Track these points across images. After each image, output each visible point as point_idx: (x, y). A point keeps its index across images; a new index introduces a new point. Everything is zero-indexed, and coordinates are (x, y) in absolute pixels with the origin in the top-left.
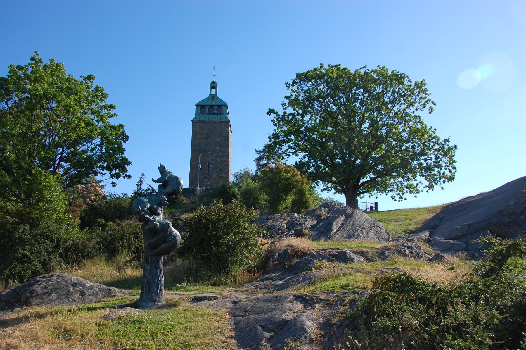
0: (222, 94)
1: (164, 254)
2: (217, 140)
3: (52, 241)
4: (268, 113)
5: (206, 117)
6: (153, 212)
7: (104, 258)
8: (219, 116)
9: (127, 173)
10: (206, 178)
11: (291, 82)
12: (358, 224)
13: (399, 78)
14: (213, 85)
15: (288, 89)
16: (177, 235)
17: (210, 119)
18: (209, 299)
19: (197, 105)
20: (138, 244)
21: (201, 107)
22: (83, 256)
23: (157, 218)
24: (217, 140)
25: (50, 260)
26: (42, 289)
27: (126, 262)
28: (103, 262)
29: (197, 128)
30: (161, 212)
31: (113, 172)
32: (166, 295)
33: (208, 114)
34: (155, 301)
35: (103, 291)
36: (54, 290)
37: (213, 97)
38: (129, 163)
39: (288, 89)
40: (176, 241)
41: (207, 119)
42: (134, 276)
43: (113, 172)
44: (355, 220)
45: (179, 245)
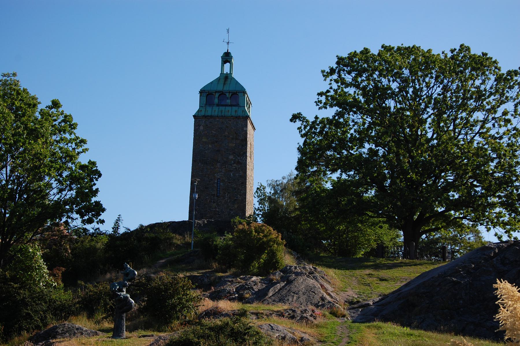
0: (241, 74)
2: (230, 145)
3: (46, 303)
4: (291, 120)
5: (215, 111)
8: (234, 108)
10: (214, 202)
11: (328, 70)
12: (294, 289)
13: (481, 64)
14: (227, 58)
15: (325, 80)
17: (220, 114)
19: (202, 92)
21: (207, 94)
22: (70, 314)
23: (122, 293)
24: (230, 145)
25: (46, 317)
27: (103, 318)
28: (85, 318)
29: (202, 128)
31: (86, 218)
32: (126, 334)
33: (218, 105)
34: (120, 336)
36: (67, 331)
37: (226, 78)
39: (325, 80)
41: (216, 114)
43: (86, 218)
44: (292, 286)
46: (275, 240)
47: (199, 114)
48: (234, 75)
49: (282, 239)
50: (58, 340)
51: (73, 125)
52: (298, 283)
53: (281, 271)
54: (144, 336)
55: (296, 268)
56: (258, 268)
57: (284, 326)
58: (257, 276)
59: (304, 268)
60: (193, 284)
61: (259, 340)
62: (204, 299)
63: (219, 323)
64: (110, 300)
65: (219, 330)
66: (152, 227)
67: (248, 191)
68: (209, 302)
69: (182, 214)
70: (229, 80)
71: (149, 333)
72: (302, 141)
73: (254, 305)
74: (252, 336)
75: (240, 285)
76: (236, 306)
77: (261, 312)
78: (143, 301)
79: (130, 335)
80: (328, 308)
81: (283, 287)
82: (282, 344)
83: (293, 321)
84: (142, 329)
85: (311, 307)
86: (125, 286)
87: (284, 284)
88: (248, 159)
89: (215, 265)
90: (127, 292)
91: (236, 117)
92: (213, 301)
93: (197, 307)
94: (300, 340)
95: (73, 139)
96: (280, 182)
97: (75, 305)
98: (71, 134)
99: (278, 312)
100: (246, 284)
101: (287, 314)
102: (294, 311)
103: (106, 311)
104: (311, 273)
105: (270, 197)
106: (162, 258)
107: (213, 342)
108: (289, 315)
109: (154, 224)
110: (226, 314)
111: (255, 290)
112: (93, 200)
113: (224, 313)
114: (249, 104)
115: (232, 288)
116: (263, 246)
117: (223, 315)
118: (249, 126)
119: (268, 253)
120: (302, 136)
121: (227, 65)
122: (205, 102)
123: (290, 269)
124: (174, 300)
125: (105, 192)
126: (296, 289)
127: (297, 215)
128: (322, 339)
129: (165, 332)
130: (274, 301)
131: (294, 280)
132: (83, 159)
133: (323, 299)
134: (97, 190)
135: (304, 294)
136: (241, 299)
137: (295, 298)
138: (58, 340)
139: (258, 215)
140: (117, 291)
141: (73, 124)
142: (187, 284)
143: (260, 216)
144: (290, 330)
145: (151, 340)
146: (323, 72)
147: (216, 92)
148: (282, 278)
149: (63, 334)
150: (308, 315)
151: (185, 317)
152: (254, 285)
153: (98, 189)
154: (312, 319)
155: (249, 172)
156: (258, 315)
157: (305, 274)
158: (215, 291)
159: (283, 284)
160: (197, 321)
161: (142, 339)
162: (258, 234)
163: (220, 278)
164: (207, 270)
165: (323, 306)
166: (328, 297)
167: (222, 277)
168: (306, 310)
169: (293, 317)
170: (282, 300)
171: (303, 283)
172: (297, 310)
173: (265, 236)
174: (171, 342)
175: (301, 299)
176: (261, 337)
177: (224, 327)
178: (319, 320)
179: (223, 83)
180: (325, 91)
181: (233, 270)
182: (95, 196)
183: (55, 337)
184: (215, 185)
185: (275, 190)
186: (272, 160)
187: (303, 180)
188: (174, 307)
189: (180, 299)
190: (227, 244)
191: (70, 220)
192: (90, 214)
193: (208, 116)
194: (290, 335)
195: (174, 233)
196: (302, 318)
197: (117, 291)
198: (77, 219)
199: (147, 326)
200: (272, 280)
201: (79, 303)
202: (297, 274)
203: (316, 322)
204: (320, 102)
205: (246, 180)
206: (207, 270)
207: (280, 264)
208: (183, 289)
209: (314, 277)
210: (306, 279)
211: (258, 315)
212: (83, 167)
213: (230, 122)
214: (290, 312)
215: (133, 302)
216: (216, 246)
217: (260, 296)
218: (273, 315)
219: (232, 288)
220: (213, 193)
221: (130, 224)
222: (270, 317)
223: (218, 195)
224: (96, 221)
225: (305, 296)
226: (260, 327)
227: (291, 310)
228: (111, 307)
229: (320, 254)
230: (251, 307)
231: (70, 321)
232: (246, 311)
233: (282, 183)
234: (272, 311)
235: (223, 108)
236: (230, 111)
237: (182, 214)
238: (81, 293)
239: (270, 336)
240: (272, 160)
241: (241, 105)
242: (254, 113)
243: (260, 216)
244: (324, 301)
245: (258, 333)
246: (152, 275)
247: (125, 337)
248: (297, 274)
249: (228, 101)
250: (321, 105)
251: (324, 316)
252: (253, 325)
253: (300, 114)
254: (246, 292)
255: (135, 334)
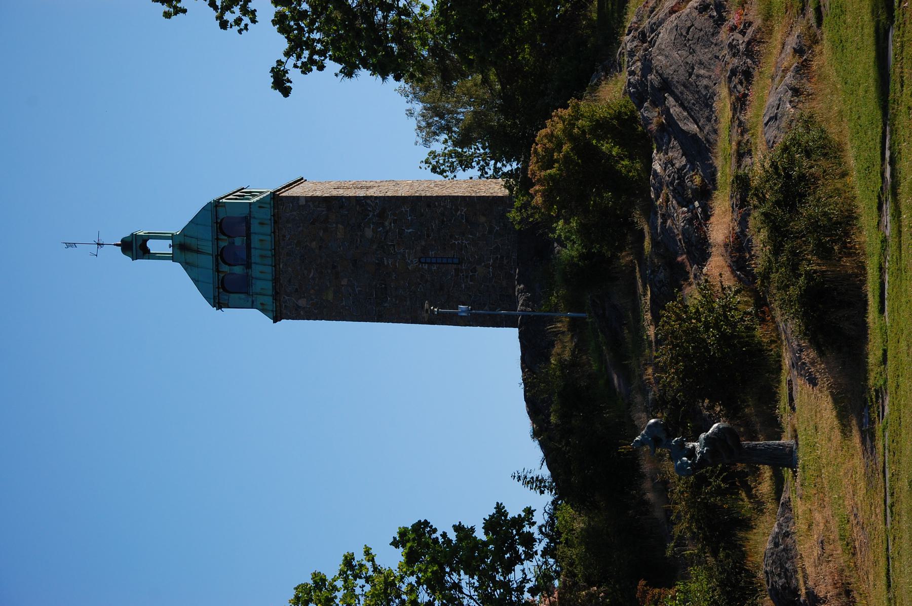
1: (739, 441)
4: (286, 92)
5: (262, 275)
6: (691, 453)
8: (255, 227)
12: (682, 75)
14: (135, 247)
16: (718, 427)
17: (269, 261)
19: (218, 304)
20: (717, 477)
21: (223, 292)
22: (742, 569)
23: (698, 449)
26: (780, 578)
27: (750, 496)
29: (302, 302)
30: (691, 445)
31: (521, 549)
32: (786, 440)
33: (248, 265)
36: (782, 567)
37: (184, 248)
40: (723, 428)
41: (269, 269)
42: (771, 479)
44: (676, 78)
46: (569, 124)
48: (177, 229)
49: (566, 107)
50: (801, 582)
52: (667, 67)
53: (640, 106)
54: (791, 399)
55: (632, 73)
56: (631, 158)
57: (768, 94)
58: (651, 160)
59: (632, 54)
61: (800, 145)
63: (764, 234)
64: (710, 483)
65: (779, 233)
66: (536, 406)
67: (445, 193)
68: (713, 264)
69: (505, 342)
70: (188, 241)
73: (719, 163)
74: (792, 161)
77: (734, 147)
79: (788, 431)
81: (677, 99)
83: (756, 73)
85: (724, 35)
86: (681, 445)
87: (671, 99)
88: (371, 193)
89: (626, 258)
90: (696, 439)
91: (275, 222)
92: (709, 255)
93: (723, 289)
96: (420, 118)
98: (335, 588)
99: (734, 109)
100: (672, 183)
101: (739, 87)
102: (734, 72)
103: (732, 490)
104: (643, 37)
106: (610, 381)
108: (741, 83)
109: (528, 406)
110: (740, 223)
111: (683, 163)
112: (480, 534)
113: (737, 229)
114: (242, 193)
115: (681, 214)
118: (296, 191)
121: (152, 245)
122: (243, 296)
123: (634, 86)
125: (458, 509)
126: (682, 70)
127: (497, 75)
129: (780, 356)
130: (709, 119)
131: (660, 75)
132: (392, 559)
134: (458, 528)
135: (692, 52)
136: (705, 193)
137: (702, 72)
138: (801, 582)
139: (496, 170)
140: (694, 461)
141: (315, 582)
142: (674, 312)
143: (499, 165)
144: (778, 78)
147: (218, 271)
148: (654, 104)
149: (788, 575)
150: (741, 41)
151: (746, 313)
152: (673, 165)
153: (454, 526)
154: (750, 32)
155: (403, 192)
157: (646, 50)
159: (671, 101)
161: (797, 402)
163: (655, 243)
164: (638, 275)
167: (653, 240)
168: (731, 46)
169: (748, 75)
170: (707, 101)
171: (667, 56)
172: (730, 67)
174: (805, 334)
175: (705, 58)
177: (774, 222)
179: (195, 255)
180: (214, 14)
183: (795, 592)
184: (435, 268)
186: (370, 137)
187: (421, 65)
188: (724, 339)
189: (707, 326)
190: (578, 231)
191: (528, 586)
193: (274, 288)
194: (789, 79)
195: (548, 360)
196: (749, 53)
197: (694, 461)
198: (523, 571)
199: (769, 397)
200: (661, 125)
201: (715, 554)
202: (647, 67)
203: (758, 22)
205: (420, 197)
206: (638, 275)
207: (623, 109)
208: (684, 321)
210: (659, 49)
212: (411, 558)
213: (288, 237)
214: (735, 80)
217: (698, 151)
218: (742, 118)
219: (681, 214)
220: (453, 272)
221: (532, 458)
223: (456, 261)
225: (698, 48)
226: (770, 145)
227: (730, 78)
229: (591, 19)
230: (725, 171)
232: (737, 177)
234: (732, 121)
236: (262, 237)
237: (505, 342)
239: (792, 121)
240: (370, 137)
242: (264, 182)
243: (499, 165)
245: (785, 149)
246: (650, 396)
247: (793, 441)
248: (647, 67)
249: (238, 241)
252: (767, 160)
254: (689, 184)
255: (786, 420)
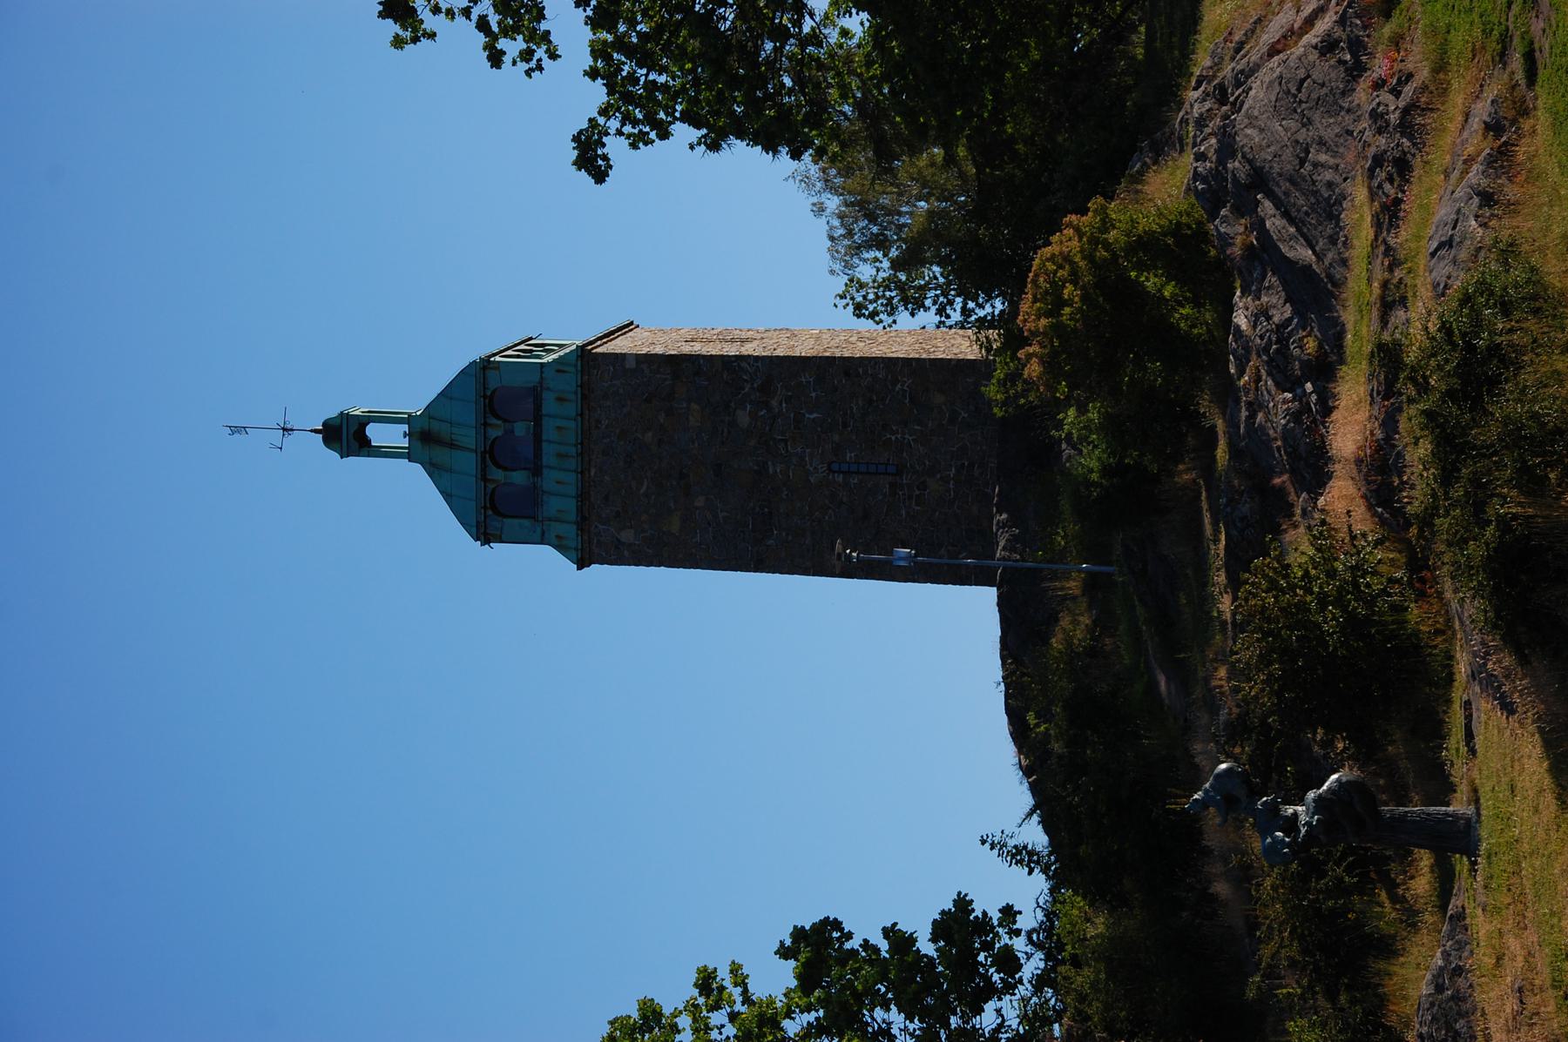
4: (600, 176)
5: (560, 484)
6: (1291, 824)
7: (1382, 965)
8: (549, 405)
9: (995, 916)
14: (347, 435)
15: (432, 36)
16: (1338, 780)
18: (1469, 718)
19: (485, 535)
21: (493, 515)
23: (1303, 818)
27: (1395, 899)
29: (627, 536)
30: (1290, 810)
32: (1459, 806)
33: (537, 470)
35: (1453, 930)
36: (1449, 1027)
37: (428, 439)
38: (963, 903)
40: (1348, 782)
41: (571, 478)
44: (1277, 169)
45: (1356, 773)
47: (572, 544)
48: (417, 407)
49: (1083, 211)
51: (644, 1017)
53: (1213, 215)
55: (1200, 157)
56: (1197, 304)
57: (1437, 201)
58: (1230, 309)
59: (1201, 123)
60: (1266, 554)
61: (1492, 294)
62: (1323, 511)
63: (1424, 449)
65: (1451, 449)
67: (876, 352)
68: (1335, 492)
69: (968, 617)
70: (435, 426)
71: (1457, 716)
72: (684, 133)
73: (1349, 317)
74: (1477, 322)
75: (1269, 374)
76: (1353, 394)
78: (1328, 744)
80: (1365, 27)
81: (1278, 204)
82: (1509, 204)
83: (1417, 162)
84: (1440, 748)
85: (1362, 95)
86: (1273, 809)
87: (1268, 204)
88: (749, 349)
89: (1185, 475)
90: (1300, 801)
91: (584, 397)
92: (1330, 476)
93: (1353, 538)
94: (1497, 137)
95: (695, 1020)
96: (836, 223)
97: (1342, 1010)
99: (1377, 225)
100: (1266, 349)
101: (1387, 186)
102: (1378, 161)
104: (1221, 95)
105: (896, 265)
106: (1153, 685)
107: (1499, 466)
108: (1391, 180)
110: (1383, 425)
111: (1288, 315)
112: (926, 947)
113: (1379, 434)
114: (530, 347)
115: (1279, 406)
116: (1109, 283)
117: (1388, 439)
118: (620, 345)
119: (1141, 267)
120: (664, 135)
122: (526, 522)
123: (1204, 180)
124: (1330, 621)
125: (889, 902)
126: (1288, 154)
128: (1493, 46)
129: (1451, 658)
130: (1333, 240)
131: (1250, 162)
132: (774, 979)
133: (1328, 46)
135: (1307, 123)
136: (1325, 369)
137: (1323, 158)
139: (966, 312)
140: (1295, 839)
144: (1456, 174)
145: (1485, 708)
146: (398, 43)
147: (485, 479)
148: (1239, 211)
150: (1393, 106)
151: (1391, 581)
152: (1269, 318)
153: (885, 930)
154: (1408, 90)
155: (804, 349)
156: (1391, 301)
158: (1293, 472)
159: (1267, 207)
160: (1414, 531)
162: (1069, 303)
163: (1235, 452)
164: (1205, 506)
165: (1356, 46)
166: (1323, 25)
168: (1375, 115)
170: (1331, 209)
171: (1263, 129)
172: (1372, 151)
173: (1074, 278)
174: (1495, 626)
175: (1328, 135)
176: (1484, 287)
178: (1419, 62)
180: (481, 39)
181: (1205, 404)
182: (911, 940)
185: (868, 246)
186: (747, 255)
188: (1353, 625)
189: (1323, 601)
192: (981, 958)
193: (580, 510)
194: (1475, 176)
197: (1295, 839)
200: (1249, 248)
201: (1332, 997)
202: (1228, 148)
203: (1423, 74)
204: (527, 55)
205: (832, 359)
206: (1205, 506)
207: (1184, 219)
209: (1238, 84)
210: (1248, 116)
211: (1391, 301)
212: (808, 980)
214: (1381, 175)
215: (1334, 777)
216: (1106, 471)
217: (1314, 294)
218: (1391, 241)
219: (1279, 406)
222: (1401, 255)
224: (1006, 939)
225: (1316, 117)
226: (1440, 291)
227: (1371, 170)
228: (1349, 870)
229: (1134, 58)
231: (1407, 1025)
232: (1381, 347)
233: (841, 216)
234: (1374, 246)
235: (549, 453)
237: (968, 617)
238: (1290, 988)
240: (747, 255)
241: (537, 378)
242: (566, 329)
244: (1338, 41)
245: (1466, 299)
246: (1223, 717)
247: (1472, 808)
248: (1228, 148)
249: (521, 429)
250: (540, 53)
251: (1397, 41)
253: (576, 139)
254: (1297, 352)
255: (1459, 771)
